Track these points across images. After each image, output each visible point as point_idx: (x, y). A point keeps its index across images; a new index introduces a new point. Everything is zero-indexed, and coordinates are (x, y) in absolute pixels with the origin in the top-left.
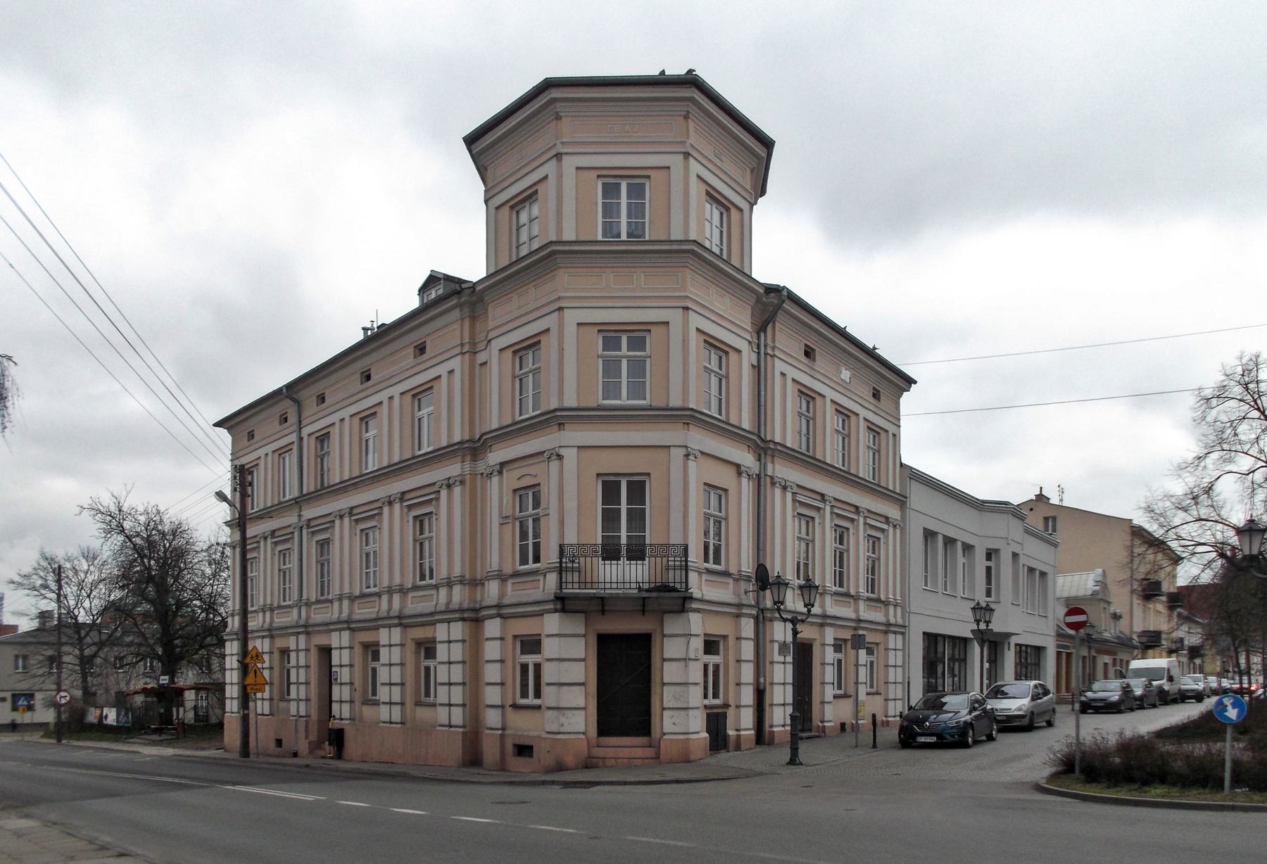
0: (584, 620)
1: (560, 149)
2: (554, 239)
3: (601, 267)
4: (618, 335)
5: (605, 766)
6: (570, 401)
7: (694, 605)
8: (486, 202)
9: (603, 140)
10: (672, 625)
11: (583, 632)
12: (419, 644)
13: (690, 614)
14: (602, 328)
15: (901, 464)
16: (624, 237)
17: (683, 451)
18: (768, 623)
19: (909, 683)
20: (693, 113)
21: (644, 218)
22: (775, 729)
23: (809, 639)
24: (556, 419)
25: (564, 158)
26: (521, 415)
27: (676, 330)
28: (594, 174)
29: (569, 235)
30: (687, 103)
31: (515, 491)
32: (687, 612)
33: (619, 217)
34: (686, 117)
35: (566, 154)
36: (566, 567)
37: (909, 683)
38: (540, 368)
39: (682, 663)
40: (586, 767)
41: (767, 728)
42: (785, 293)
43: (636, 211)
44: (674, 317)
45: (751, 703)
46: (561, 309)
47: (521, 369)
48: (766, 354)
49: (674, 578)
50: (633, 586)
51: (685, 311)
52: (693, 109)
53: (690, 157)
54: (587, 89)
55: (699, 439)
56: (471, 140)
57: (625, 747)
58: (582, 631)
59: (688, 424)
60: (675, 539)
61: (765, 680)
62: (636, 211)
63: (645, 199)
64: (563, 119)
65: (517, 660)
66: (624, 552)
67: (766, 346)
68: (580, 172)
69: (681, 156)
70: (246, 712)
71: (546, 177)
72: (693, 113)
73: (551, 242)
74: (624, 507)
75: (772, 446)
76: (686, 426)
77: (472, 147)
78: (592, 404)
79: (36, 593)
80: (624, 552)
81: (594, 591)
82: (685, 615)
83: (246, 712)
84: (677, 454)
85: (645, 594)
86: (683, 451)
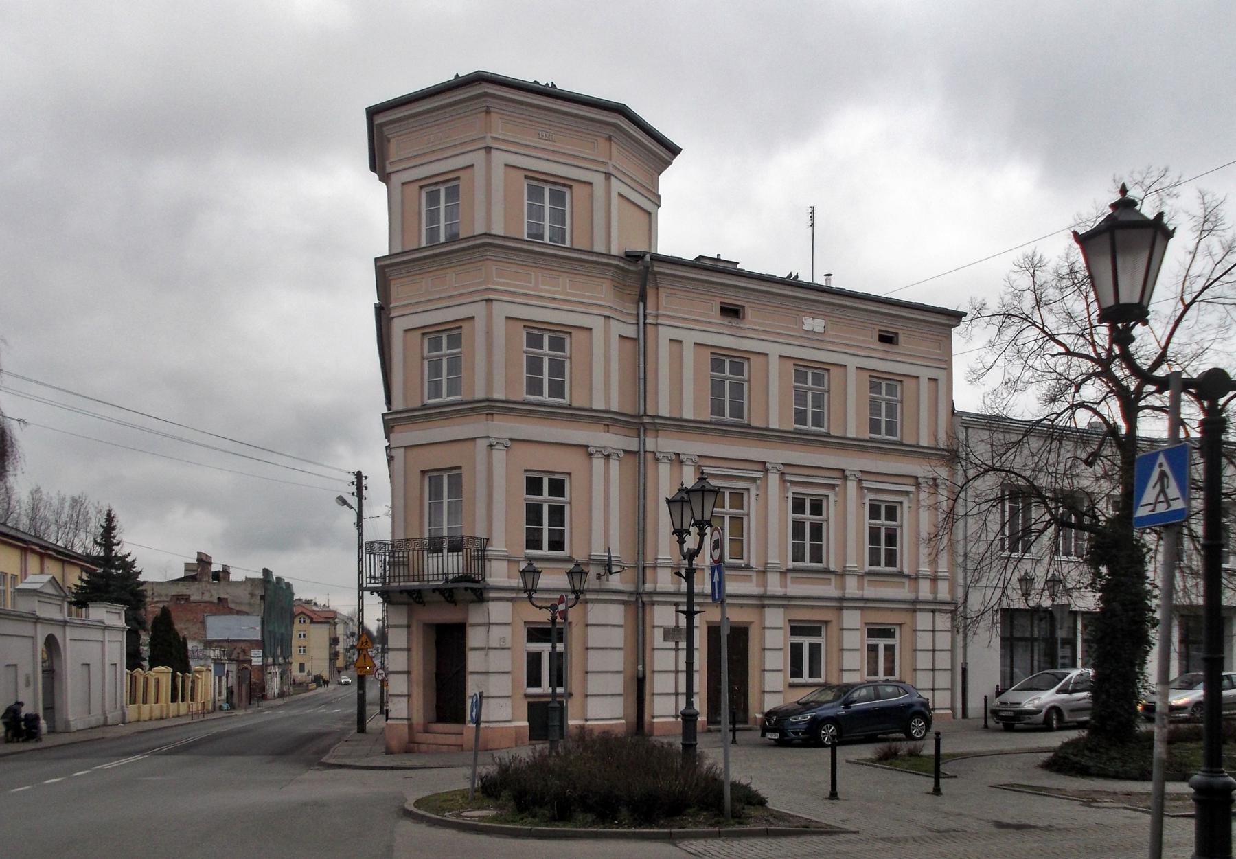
0: (406, 615)
3: (420, 274)
5: (420, 752)
6: (498, 395)
7: (492, 595)
10: (475, 615)
11: (405, 622)
13: (491, 603)
15: (953, 412)
17: (485, 442)
18: (648, 608)
19: (964, 671)
22: (655, 720)
23: (743, 622)
27: (598, 335)
29: (498, 229)
30: (484, 99)
32: (488, 601)
34: (488, 112)
35: (394, 172)
36: (399, 562)
37: (964, 671)
39: (482, 653)
40: (406, 752)
41: (647, 718)
42: (648, 258)
44: (478, 310)
45: (620, 690)
48: (645, 324)
49: (475, 569)
50: (441, 577)
51: (490, 303)
52: (491, 103)
55: (504, 427)
57: (445, 733)
58: (404, 621)
59: (492, 414)
60: (480, 532)
61: (644, 668)
66: (445, 545)
67: (645, 316)
69: (483, 152)
70: (361, 692)
74: (445, 500)
75: (646, 420)
76: (489, 417)
80: (445, 545)
81: (417, 583)
82: (485, 604)
83: (361, 692)
84: (482, 445)
85: (450, 585)
86: (485, 442)
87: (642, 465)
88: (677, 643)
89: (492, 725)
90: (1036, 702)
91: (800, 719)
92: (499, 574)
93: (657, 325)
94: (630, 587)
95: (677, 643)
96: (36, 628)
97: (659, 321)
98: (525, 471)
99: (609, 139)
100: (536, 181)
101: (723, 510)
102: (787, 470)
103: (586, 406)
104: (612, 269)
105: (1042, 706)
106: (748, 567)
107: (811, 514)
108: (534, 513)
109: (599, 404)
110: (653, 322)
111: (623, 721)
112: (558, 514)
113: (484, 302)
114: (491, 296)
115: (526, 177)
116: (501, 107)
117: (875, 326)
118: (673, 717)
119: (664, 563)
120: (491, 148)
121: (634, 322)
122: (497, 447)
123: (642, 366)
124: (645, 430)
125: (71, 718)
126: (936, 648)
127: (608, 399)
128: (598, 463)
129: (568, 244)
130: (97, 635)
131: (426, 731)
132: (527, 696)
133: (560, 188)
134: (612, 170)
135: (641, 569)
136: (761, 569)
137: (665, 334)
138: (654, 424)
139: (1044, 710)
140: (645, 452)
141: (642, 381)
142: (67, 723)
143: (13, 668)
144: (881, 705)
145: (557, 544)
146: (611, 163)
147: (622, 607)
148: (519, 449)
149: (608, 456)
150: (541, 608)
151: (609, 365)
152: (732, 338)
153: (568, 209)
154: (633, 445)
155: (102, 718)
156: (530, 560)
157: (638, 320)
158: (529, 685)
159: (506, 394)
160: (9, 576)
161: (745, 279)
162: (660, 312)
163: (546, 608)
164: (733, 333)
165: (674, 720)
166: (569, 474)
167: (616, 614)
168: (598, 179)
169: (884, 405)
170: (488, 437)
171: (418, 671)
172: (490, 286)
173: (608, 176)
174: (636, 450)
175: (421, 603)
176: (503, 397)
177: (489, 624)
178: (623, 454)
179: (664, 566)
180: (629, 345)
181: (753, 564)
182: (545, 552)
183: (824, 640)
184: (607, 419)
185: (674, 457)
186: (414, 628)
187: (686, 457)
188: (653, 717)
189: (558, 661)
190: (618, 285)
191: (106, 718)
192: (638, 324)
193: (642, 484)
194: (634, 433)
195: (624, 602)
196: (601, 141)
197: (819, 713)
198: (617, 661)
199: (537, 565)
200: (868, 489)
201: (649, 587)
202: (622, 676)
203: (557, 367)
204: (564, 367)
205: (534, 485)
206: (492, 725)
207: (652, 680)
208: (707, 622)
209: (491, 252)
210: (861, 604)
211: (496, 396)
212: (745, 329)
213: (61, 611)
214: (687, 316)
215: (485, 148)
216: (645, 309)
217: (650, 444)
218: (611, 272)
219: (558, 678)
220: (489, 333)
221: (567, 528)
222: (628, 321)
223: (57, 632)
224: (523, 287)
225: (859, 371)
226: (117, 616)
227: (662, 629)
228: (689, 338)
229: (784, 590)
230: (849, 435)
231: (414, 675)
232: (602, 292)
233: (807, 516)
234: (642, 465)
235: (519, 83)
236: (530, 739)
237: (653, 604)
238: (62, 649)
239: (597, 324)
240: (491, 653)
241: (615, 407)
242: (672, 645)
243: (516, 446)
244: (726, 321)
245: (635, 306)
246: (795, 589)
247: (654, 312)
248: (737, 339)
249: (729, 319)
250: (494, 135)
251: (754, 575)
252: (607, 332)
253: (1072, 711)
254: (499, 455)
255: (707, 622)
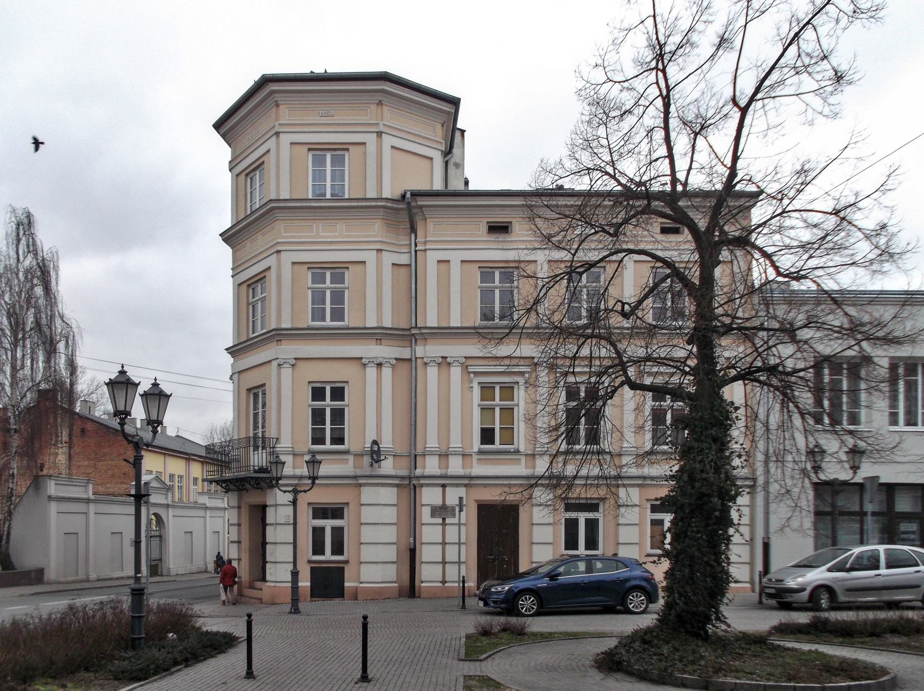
1: (278, 129)
2: (273, 197)
4: (511, 270)
6: (286, 324)
8: (230, 170)
9: (354, 122)
12: (253, 507)
14: (311, 266)
16: (328, 196)
19: (766, 546)
20: (280, 99)
21: (344, 182)
24: (278, 335)
25: (281, 135)
26: (253, 333)
27: (371, 267)
28: (306, 148)
29: (285, 195)
31: (249, 390)
33: (325, 181)
34: (278, 105)
37: (766, 546)
38: (265, 297)
43: (338, 176)
46: (278, 252)
47: (253, 298)
48: (416, 251)
51: (379, 252)
52: (277, 97)
53: (383, 134)
54: (302, 83)
55: (289, 350)
56: (218, 126)
62: (338, 176)
63: (344, 167)
64: (281, 106)
65: (310, 524)
68: (293, 146)
71: (269, 151)
72: (280, 99)
73: (271, 200)
75: (414, 331)
77: (219, 130)
78: (305, 326)
79: (877, 447)
81: (244, 473)
87: (414, 370)
88: (444, 519)
89: (278, 585)
90: (800, 580)
91: (500, 589)
92: (293, 468)
93: (425, 250)
94: (404, 472)
95: (444, 519)
96: (88, 506)
97: (428, 247)
98: (309, 382)
99: (380, 103)
100: (317, 150)
101: (512, 402)
102: (470, 362)
103: (362, 326)
104: (382, 210)
105: (808, 584)
106: (517, 452)
107: (331, 400)
108: (318, 416)
109: (371, 322)
110: (422, 248)
111: (396, 585)
112: (338, 416)
113: (276, 254)
114: (279, 248)
115: (309, 150)
116: (314, 99)
117: (482, 219)
118: (441, 582)
119: (431, 451)
120: (382, 132)
121: (408, 251)
122: (285, 366)
123: (413, 286)
124: (416, 340)
125: (171, 567)
126: (441, 527)
127: (379, 317)
128: (371, 371)
129: (346, 196)
130: (201, 513)
131: (252, 587)
132: (310, 562)
133: (339, 150)
134: (382, 128)
135: (413, 458)
136: (529, 452)
137: (432, 257)
138: (423, 334)
139: (809, 589)
140: (416, 358)
141: (413, 299)
142: (169, 569)
143: (75, 535)
144: (592, 579)
145: (338, 439)
146: (381, 123)
147: (395, 489)
148: (302, 365)
149: (380, 365)
150: (285, 492)
151: (381, 289)
152: (500, 252)
153: (346, 168)
154: (406, 353)
155: (204, 566)
156: (313, 453)
157: (411, 249)
158: (314, 553)
159: (292, 323)
160: (176, 476)
161: (469, 198)
162: (427, 239)
163: (289, 492)
164: (500, 247)
165: (441, 585)
166: (347, 382)
167: (388, 495)
168: (371, 139)
169: (497, 292)
170: (277, 359)
171: (245, 544)
172: (280, 240)
173: (380, 134)
174: (409, 357)
175: (245, 489)
176: (289, 326)
177: (276, 505)
178: (394, 362)
179: (432, 454)
180: (404, 271)
181: (522, 449)
182: (328, 446)
183: (602, 515)
184: (380, 335)
185: (440, 360)
186: (243, 509)
187: (452, 360)
188: (422, 582)
189: (338, 533)
190: (392, 222)
191: (207, 567)
192: (410, 252)
193: (413, 386)
194: (407, 343)
195: (397, 486)
196: (374, 107)
197: (517, 584)
198: (390, 534)
199: (319, 457)
200: (475, 373)
201: (418, 472)
202: (395, 547)
203: (338, 297)
204: (344, 295)
205: (318, 394)
206: (278, 585)
207: (421, 548)
208: (476, 501)
209: (278, 214)
210: (640, 482)
211: (284, 326)
212: (512, 241)
213: (167, 498)
214: (454, 239)
215: (377, 132)
216: (416, 239)
217: (420, 351)
218: (381, 212)
219: (338, 548)
220: (279, 277)
221: (346, 426)
222: (402, 251)
223: (162, 512)
224: (302, 237)
225: (395, 267)
226: (221, 501)
227: (429, 508)
228: (455, 257)
229: (532, 470)
230: (453, 324)
231: (243, 544)
232: (375, 230)
233: (328, 403)
234: (414, 370)
235: (273, 77)
236: (311, 597)
237: (422, 486)
238: (166, 525)
239: (370, 257)
240: (279, 527)
241: (387, 323)
242: (440, 521)
243: (300, 363)
244: (493, 237)
245: (408, 237)
246: (479, 469)
247: (423, 240)
248: (504, 251)
249: (497, 235)
250: (281, 122)
251: (523, 459)
252: (379, 262)
253: (849, 590)
254: (287, 372)
255: (476, 501)
